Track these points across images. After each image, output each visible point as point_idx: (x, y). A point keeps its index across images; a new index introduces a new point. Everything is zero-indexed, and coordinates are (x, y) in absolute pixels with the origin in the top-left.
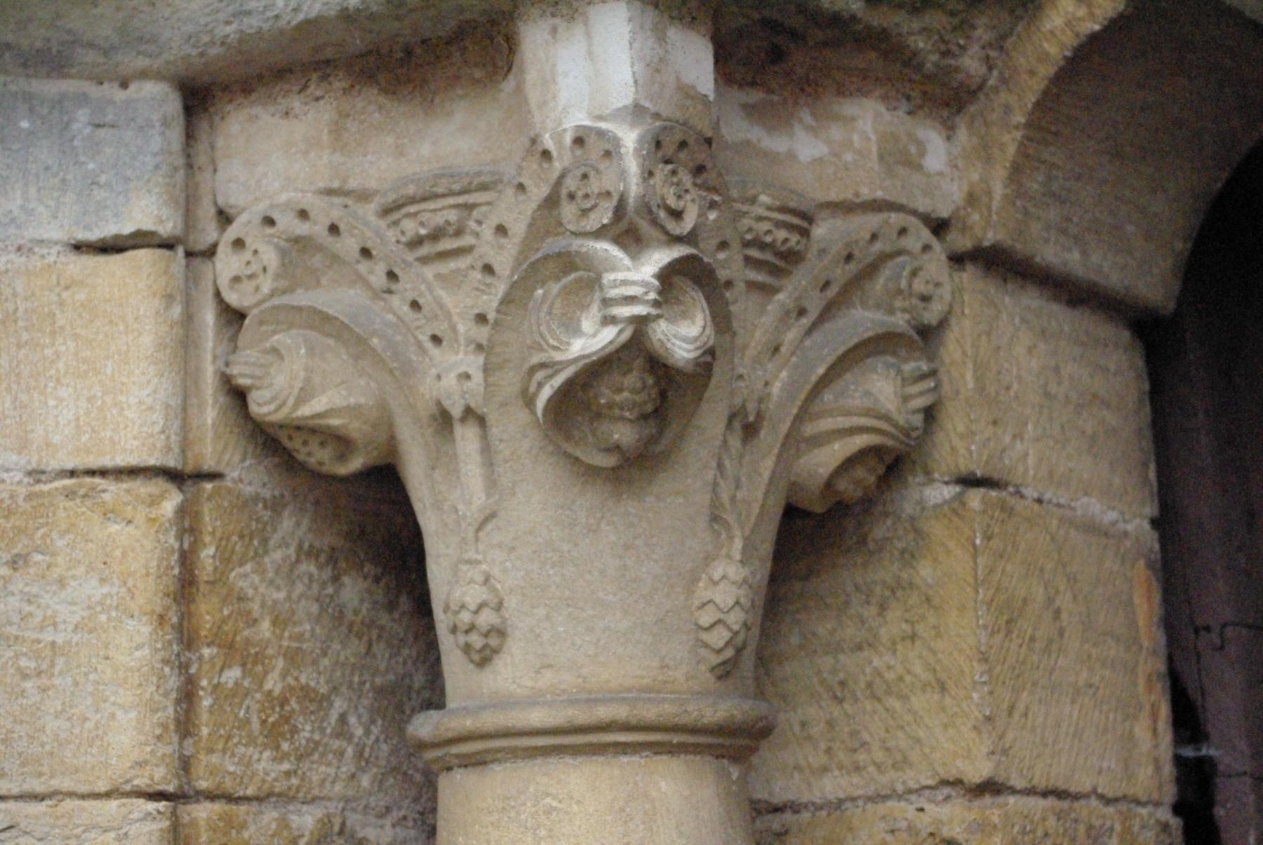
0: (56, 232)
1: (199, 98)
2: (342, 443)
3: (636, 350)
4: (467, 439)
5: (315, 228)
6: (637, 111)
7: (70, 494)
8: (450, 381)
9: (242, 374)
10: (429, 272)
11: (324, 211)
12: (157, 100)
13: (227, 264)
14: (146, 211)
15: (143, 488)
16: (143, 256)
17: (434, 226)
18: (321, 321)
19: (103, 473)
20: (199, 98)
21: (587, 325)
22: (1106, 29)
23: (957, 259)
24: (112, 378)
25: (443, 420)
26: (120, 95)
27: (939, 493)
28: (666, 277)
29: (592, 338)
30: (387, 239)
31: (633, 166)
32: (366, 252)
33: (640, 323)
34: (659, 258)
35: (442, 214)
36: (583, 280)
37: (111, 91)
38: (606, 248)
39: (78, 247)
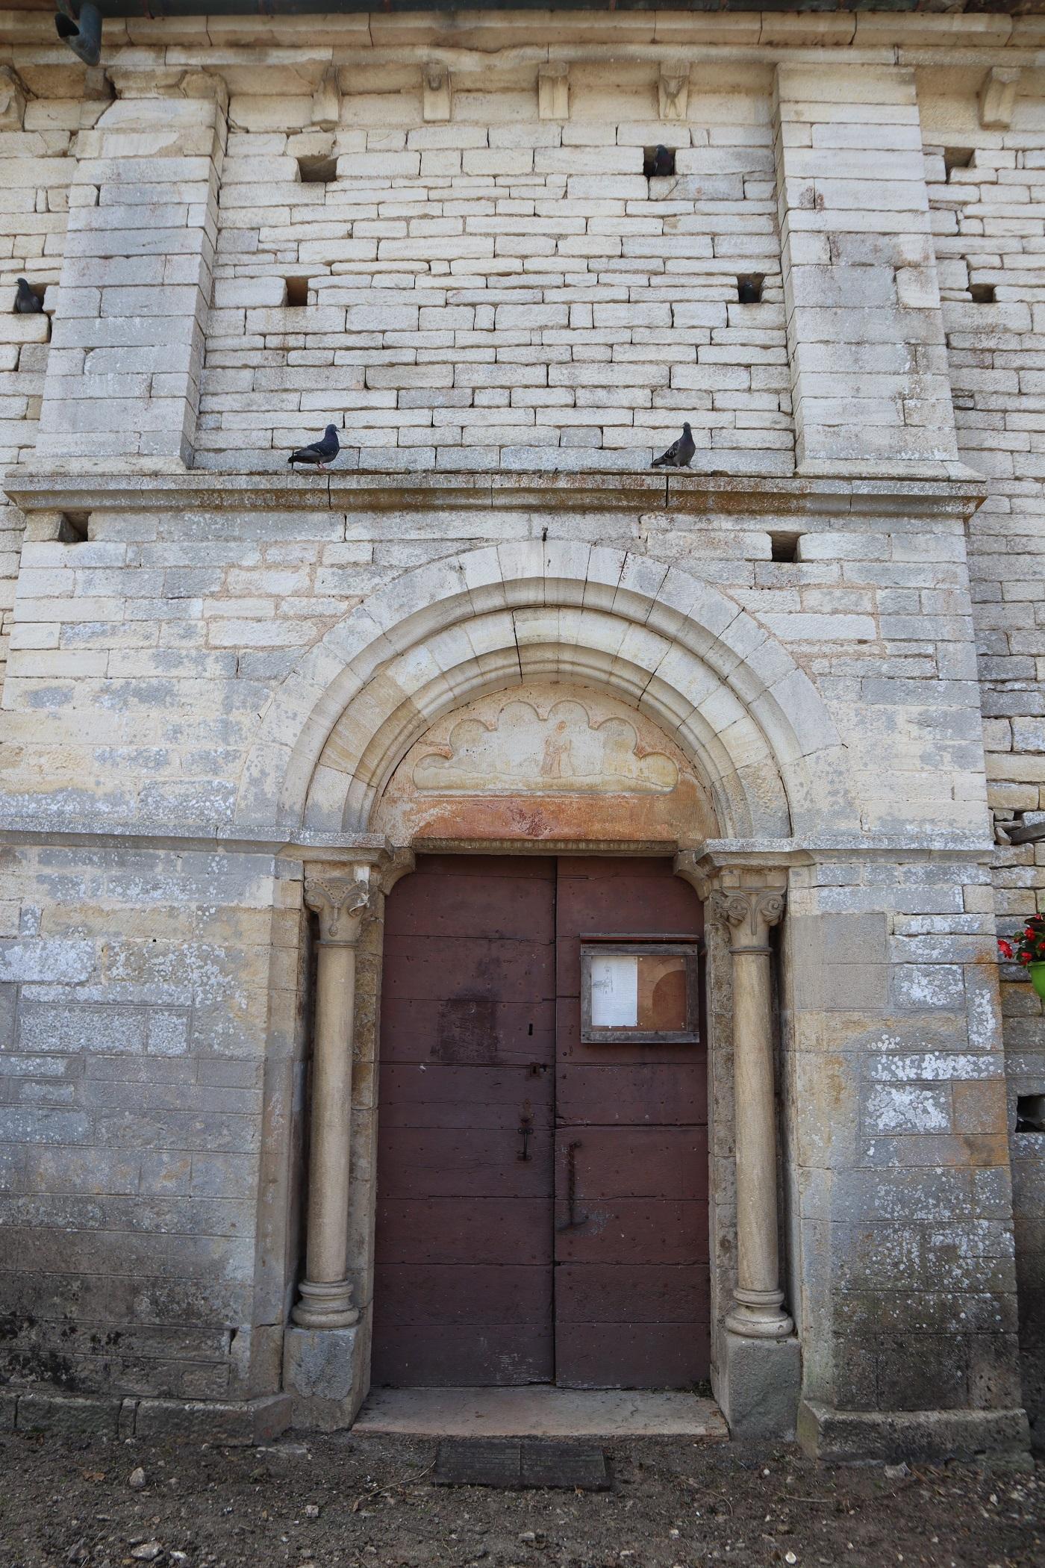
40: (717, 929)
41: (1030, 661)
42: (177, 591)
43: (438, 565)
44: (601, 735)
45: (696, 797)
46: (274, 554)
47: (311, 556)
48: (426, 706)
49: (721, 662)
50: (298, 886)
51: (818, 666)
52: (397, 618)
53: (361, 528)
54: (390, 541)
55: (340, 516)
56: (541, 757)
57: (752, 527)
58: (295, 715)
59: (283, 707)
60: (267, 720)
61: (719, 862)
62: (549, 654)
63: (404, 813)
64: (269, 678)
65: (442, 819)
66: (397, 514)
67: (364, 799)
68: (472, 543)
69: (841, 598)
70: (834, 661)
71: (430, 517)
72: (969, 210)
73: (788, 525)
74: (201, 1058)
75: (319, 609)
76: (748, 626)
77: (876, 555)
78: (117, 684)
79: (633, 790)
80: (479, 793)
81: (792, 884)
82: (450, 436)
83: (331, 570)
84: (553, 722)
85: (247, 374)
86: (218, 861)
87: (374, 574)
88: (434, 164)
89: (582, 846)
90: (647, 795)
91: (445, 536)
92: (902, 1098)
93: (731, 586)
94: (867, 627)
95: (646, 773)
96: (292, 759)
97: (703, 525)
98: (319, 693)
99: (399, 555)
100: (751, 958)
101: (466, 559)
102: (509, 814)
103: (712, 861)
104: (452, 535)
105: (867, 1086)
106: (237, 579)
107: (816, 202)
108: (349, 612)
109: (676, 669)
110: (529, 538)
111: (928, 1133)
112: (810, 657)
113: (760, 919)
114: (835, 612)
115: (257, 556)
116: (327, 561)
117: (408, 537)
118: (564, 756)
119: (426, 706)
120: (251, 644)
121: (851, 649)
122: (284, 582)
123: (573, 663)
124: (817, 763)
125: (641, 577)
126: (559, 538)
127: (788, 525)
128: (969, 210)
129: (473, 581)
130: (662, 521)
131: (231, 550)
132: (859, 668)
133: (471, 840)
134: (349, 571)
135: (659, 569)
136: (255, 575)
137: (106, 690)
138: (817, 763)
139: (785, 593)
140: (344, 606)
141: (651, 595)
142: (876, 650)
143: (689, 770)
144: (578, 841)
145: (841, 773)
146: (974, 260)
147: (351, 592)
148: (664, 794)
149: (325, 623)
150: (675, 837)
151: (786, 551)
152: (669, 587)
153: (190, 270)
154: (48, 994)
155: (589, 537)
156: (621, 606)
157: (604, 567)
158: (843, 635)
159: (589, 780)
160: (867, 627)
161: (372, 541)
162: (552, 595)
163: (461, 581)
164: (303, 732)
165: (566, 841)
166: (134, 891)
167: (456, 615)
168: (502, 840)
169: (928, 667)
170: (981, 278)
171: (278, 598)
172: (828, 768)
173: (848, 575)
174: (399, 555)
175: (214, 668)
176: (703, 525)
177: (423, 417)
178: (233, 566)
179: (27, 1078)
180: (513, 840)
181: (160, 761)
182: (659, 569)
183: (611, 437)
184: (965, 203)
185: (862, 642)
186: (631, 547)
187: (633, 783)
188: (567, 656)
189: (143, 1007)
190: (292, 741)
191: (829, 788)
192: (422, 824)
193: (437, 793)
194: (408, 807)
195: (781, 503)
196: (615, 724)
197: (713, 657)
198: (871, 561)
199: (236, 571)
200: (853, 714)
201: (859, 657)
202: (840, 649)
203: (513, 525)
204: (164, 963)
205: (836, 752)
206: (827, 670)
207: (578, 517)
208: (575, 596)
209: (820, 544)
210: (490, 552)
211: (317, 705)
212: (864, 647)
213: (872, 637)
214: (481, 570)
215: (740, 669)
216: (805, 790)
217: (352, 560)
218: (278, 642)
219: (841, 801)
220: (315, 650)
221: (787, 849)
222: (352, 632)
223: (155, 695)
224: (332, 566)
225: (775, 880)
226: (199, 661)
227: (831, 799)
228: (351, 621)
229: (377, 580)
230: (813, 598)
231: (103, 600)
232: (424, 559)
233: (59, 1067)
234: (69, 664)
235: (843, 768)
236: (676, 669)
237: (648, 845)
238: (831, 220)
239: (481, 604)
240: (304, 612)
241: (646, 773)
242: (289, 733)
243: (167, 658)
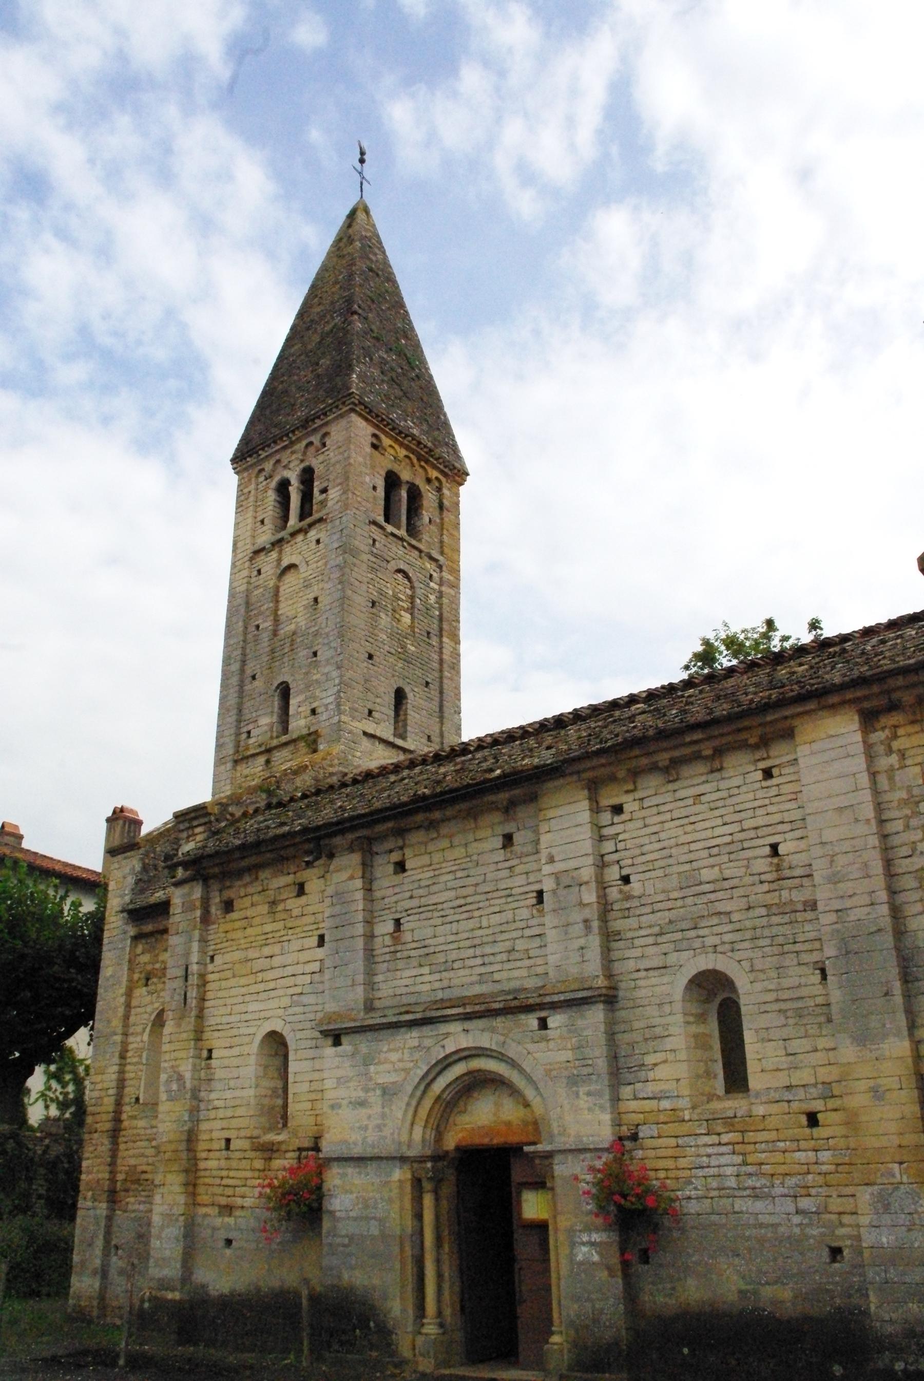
41: (640, 1056)
42: (368, 1061)
45: (536, 1127)
47: (402, 1045)
51: (554, 1073)
68: (448, 1035)
72: (621, 837)
73: (543, 1014)
74: (384, 1236)
78: (353, 1100)
82: (445, 983)
85: (386, 964)
86: (383, 1164)
88: (435, 860)
92: (585, 1249)
100: (97, 1285)
101: (445, 1042)
105: (573, 1245)
107: (551, 860)
111: (593, 1263)
112: (551, 1070)
116: (407, 1046)
121: (564, 1065)
122: (394, 1057)
125: (497, 1043)
127: (543, 1014)
128: (621, 837)
129: (448, 1051)
132: (565, 1073)
137: (350, 1103)
140: (412, 1064)
146: (622, 863)
153: (360, 929)
154: (343, 1215)
157: (485, 1041)
162: (473, 1052)
166: (363, 1176)
167: (445, 1064)
169: (590, 1070)
170: (625, 872)
175: (378, 1092)
177: (437, 976)
179: (339, 1245)
181: (366, 1128)
182: (502, 1038)
183: (496, 976)
184: (618, 834)
186: (493, 1030)
189: (368, 1219)
195: (541, 1006)
204: (371, 1202)
209: (555, 1020)
223: (362, 1104)
226: (374, 1090)
230: (552, 1044)
231: (347, 1070)
233: (346, 1241)
234: (342, 1093)
238: (559, 866)
242: (400, 1115)
243: (366, 1090)
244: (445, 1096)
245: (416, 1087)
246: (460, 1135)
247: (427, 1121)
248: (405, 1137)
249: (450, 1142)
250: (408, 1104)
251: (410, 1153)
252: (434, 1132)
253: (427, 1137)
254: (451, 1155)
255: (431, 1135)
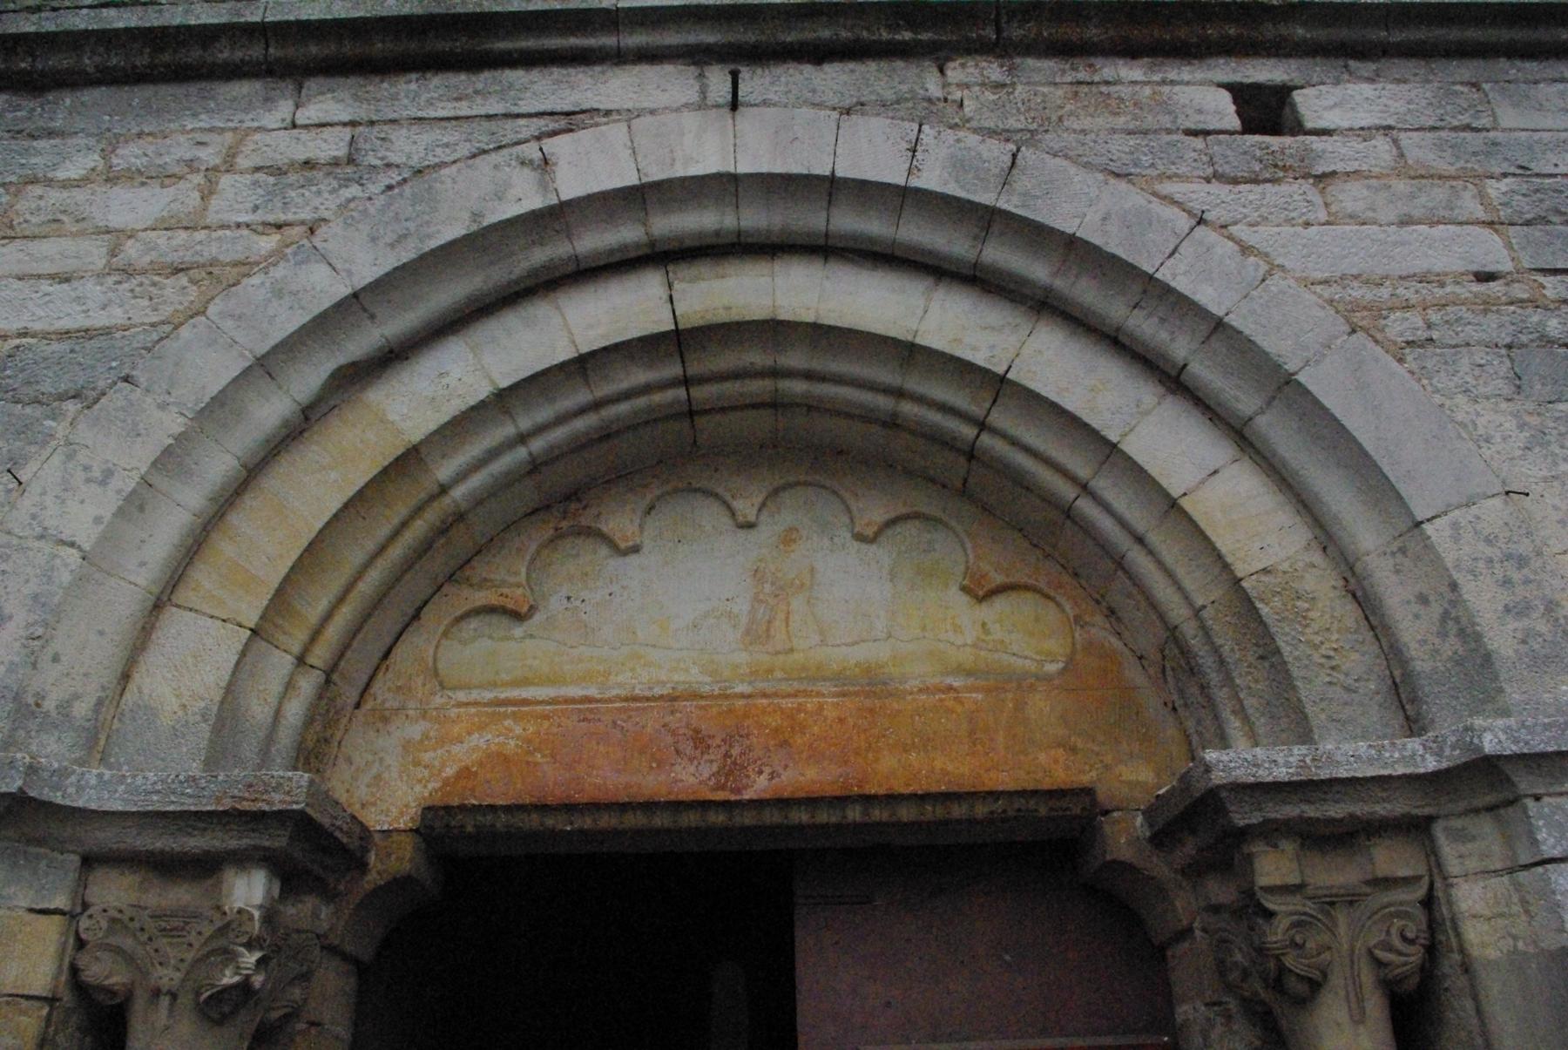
0: (25, 904)
1: (89, 862)
2: (114, 994)
3: (245, 987)
4: (165, 1001)
5: (125, 918)
6: (260, 907)
7: (8, 1003)
8: (166, 980)
9: (81, 964)
10: (165, 940)
11: (129, 913)
12: (75, 860)
13: (84, 923)
14: (61, 901)
15: (37, 1004)
16: (57, 918)
17: (173, 925)
18: (118, 951)
19: (22, 996)
20: (89, 862)
21: (227, 972)
22: (388, 884)
23: (323, 948)
24: (35, 963)
25: (157, 993)
26: (61, 857)
27: (301, 1026)
28: (259, 962)
29: (229, 978)
30: (151, 925)
31: (257, 925)
32: (142, 929)
33: (248, 977)
34: (257, 955)
35: (176, 922)
36: (229, 956)
37: (56, 855)
38: (241, 949)
39: (31, 910)
40: (1229, 1017)
43: (494, 158)
44: (881, 554)
46: (130, 155)
48: (462, 476)
49: (1164, 335)
50: (52, 928)
52: (390, 261)
53: (330, 104)
54: (393, 121)
55: (289, 86)
56: (742, 607)
57: (1186, 77)
58: (108, 474)
59: (82, 456)
60: (35, 489)
61: (1243, 816)
62: (756, 358)
63: (407, 746)
64: (62, 397)
65: (502, 759)
66: (414, 76)
67: (283, 697)
68: (571, 120)
69: (1412, 196)
70: (1434, 317)
71: (484, 79)
75: (212, 251)
76: (1219, 250)
77: (1465, 119)
79: (969, 673)
80: (593, 692)
81: (1453, 866)
83: (248, 179)
84: (768, 531)
87: (346, 182)
89: (854, 814)
90: (1006, 684)
91: (516, 110)
93: (1164, 177)
94: (1491, 250)
95: (997, 632)
96: (80, 580)
97: (1082, 75)
98: (175, 423)
99: (407, 146)
101: (559, 147)
102: (669, 739)
103: (1221, 810)
104: (524, 108)
106: (33, 205)
108: (278, 255)
109: (1052, 363)
110: (702, 105)
112: (1378, 311)
113: (1367, 977)
114: (1406, 221)
115: (94, 160)
117: (433, 114)
118: (797, 603)
119: (462, 476)
120: (37, 326)
122: (130, 207)
123: (809, 376)
124: (1456, 539)
125: (958, 165)
126: (765, 103)
130: (994, 70)
131: (39, 153)
132: (1493, 327)
133: (570, 808)
134: (293, 177)
135: (997, 152)
136: (80, 195)
138: (1456, 539)
139: (1284, 188)
141: (986, 198)
142: (1520, 291)
143: (1099, 619)
144: (841, 801)
145: (1522, 562)
147: (290, 217)
148: (1048, 678)
149: (218, 277)
150: (1086, 779)
151: (1265, 111)
152: (1022, 182)
155: (834, 100)
156: (916, 232)
158: (1440, 262)
159: (860, 654)
160: (1491, 250)
161: (353, 124)
162: (754, 218)
163: (544, 186)
164: (120, 513)
165: (812, 802)
168: (650, 806)
171: (117, 237)
172: (1489, 551)
173: (1413, 154)
174: (407, 146)
176: (1082, 75)
178: (34, 181)
180: (677, 806)
182: (997, 152)
185: (1485, 277)
187: (966, 657)
188: (795, 359)
190: (87, 536)
191: (1504, 597)
192: (449, 772)
193: (488, 695)
194: (415, 731)
196: (910, 529)
197: (1146, 326)
198: (1455, 129)
199: (37, 190)
200: (1510, 425)
201: (1487, 306)
202: (1439, 292)
203: (667, 86)
205: (1493, 510)
206: (1422, 334)
207: (808, 69)
208: (810, 219)
210: (616, 133)
211: (167, 452)
212: (1495, 287)
213: (1506, 266)
214: (589, 166)
215: (1215, 343)
216: (1436, 610)
217: (302, 157)
218: (99, 320)
219: (1542, 627)
220: (185, 332)
221: (1431, 764)
222: (278, 293)
224: (258, 169)
225: (1392, 859)
227: (1512, 624)
228: (278, 272)
229: (354, 190)
230: (1350, 196)
232: (464, 150)
235: (1524, 547)
236: (1052, 363)
237: (1019, 803)
239: (593, 241)
240: (174, 258)
241: (997, 632)
242: (84, 516)
244: (444, 471)
245: (266, 366)
246: (471, 747)
247: (281, 600)
248: (78, 668)
249: (391, 785)
250: (172, 459)
251: (91, 789)
252: (308, 684)
253: (258, 710)
254: (381, 867)
255: (280, 695)
